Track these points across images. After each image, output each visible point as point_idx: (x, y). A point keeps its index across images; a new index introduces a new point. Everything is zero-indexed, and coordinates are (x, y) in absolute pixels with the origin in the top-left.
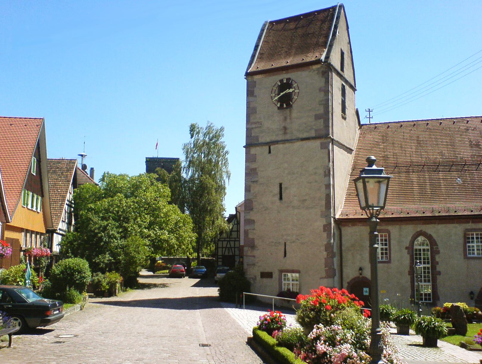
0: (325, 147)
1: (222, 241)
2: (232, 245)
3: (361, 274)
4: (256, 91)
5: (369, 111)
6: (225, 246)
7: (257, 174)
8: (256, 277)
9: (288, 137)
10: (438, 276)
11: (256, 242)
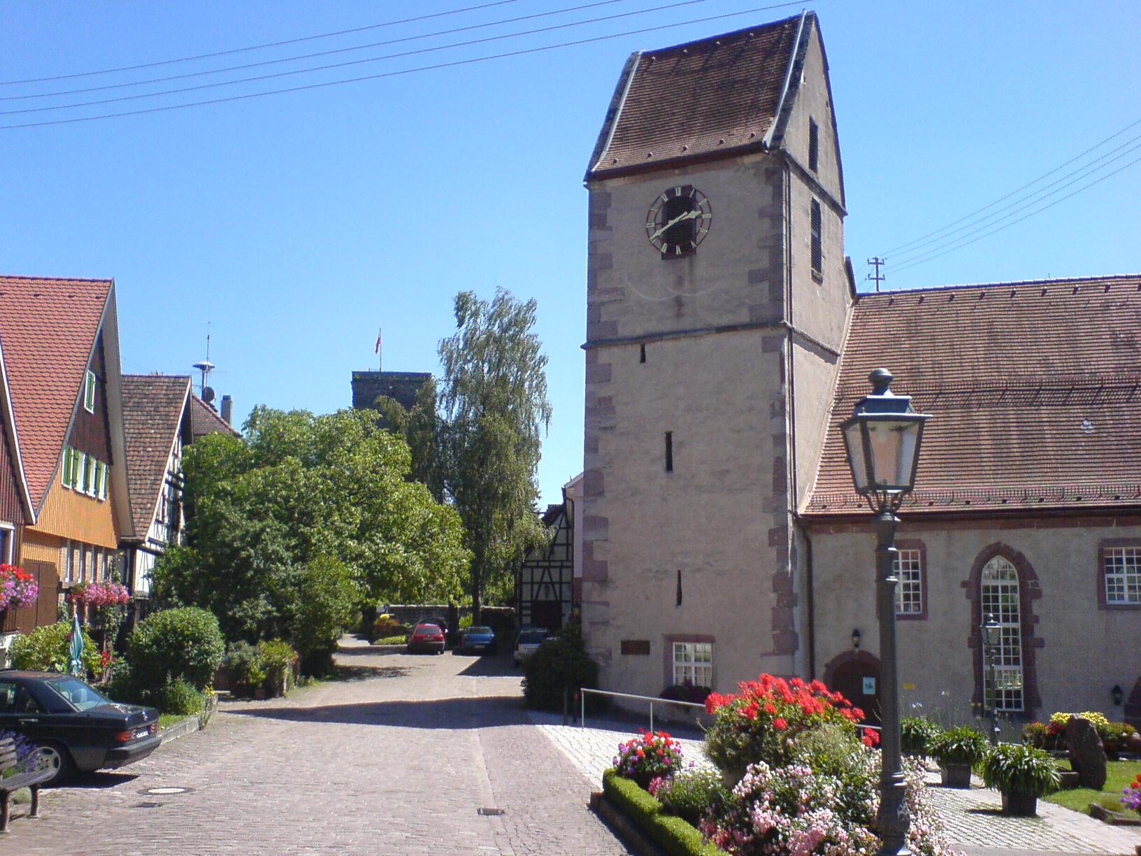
0: (772, 346)
1: (532, 568)
2: (556, 578)
3: (857, 645)
4: (612, 217)
5: (877, 263)
6: (537, 578)
7: (613, 410)
8: (610, 652)
9: (686, 324)
10: (1038, 651)
11: (612, 570)
